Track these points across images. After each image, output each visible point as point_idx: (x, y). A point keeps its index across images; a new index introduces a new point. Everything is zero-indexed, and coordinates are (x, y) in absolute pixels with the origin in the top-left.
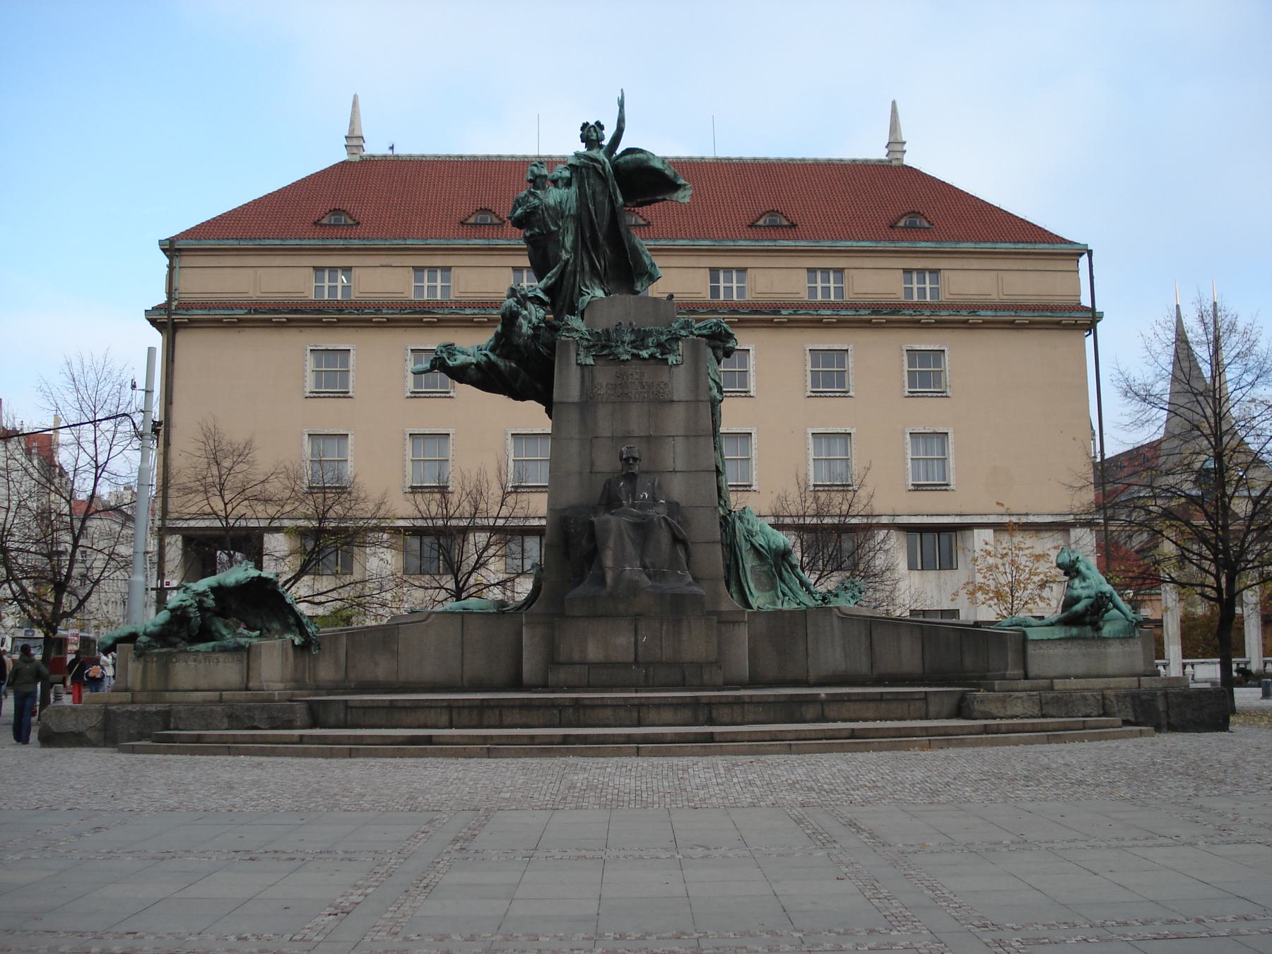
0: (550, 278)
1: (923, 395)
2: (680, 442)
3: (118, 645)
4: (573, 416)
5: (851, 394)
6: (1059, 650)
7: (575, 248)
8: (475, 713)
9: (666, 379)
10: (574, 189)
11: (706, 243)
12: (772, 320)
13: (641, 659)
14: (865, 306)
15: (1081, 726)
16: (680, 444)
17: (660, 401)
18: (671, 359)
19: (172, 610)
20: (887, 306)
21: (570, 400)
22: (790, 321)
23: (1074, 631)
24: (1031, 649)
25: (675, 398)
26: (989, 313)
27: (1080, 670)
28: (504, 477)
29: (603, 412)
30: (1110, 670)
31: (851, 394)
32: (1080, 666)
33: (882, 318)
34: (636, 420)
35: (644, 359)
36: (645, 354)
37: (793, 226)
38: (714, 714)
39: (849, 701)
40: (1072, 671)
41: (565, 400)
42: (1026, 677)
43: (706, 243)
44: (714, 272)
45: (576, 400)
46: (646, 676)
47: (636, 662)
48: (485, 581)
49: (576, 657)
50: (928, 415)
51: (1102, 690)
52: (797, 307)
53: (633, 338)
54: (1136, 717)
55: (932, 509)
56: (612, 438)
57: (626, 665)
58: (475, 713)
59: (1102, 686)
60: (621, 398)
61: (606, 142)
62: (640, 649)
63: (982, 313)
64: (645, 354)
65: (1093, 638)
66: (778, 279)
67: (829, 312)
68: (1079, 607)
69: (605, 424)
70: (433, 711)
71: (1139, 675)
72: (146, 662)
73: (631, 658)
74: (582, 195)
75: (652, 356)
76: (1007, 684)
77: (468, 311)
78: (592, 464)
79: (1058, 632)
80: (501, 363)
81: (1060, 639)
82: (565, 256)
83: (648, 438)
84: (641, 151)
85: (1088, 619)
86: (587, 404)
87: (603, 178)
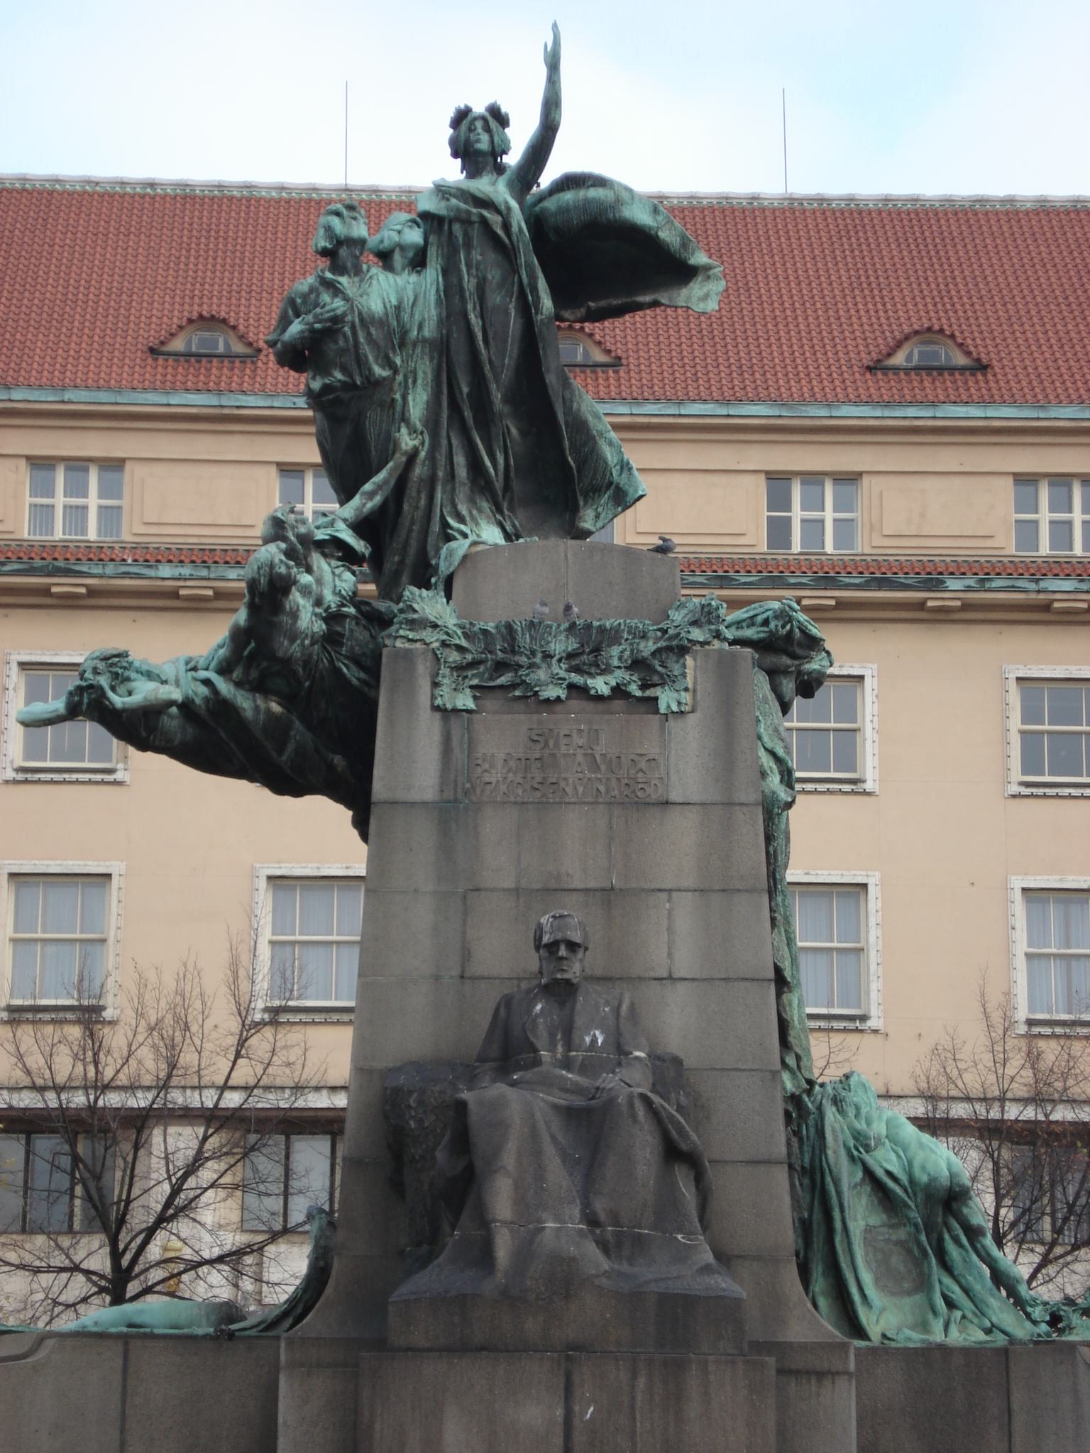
2: (685, 906)
4: (420, 837)
7: (432, 423)
9: (651, 748)
11: (759, 411)
12: (921, 605)
17: (638, 800)
18: (667, 699)
21: (415, 796)
22: (967, 606)
25: (675, 796)
28: (244, 986)
34: (578, 849)
35: (600, 698)
36: (601, 685)
37: (981, 367)
41: (401, 795)
43: (759, 411)
44: (778, 481)
48: (187, 1253)
52: (985, 572)
53: (572, 645)
60: (541, 794)
64: (601, 685)
67: (1068, 585)
69: (499, 852)
74: (451, 291)
75: (619, 692)
77: (166, 571)
78: (466, 955)
82: (407, 441)
84: (600, 182)
86: (455, 807)
87: (504, 249)
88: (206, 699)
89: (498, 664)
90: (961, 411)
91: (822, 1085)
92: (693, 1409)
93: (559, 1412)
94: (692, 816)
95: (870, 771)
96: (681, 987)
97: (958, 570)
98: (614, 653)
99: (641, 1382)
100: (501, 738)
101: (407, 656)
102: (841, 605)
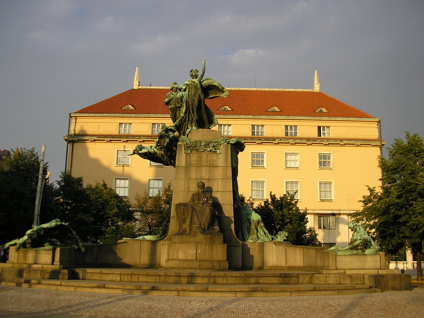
0: (177, 123)
1: (324, 169)
2: (220, 181)
3: (11, 247)
4: (183, 171)
5: (299, 168)
6: (349, 259)
7: (186, 113)
8: (129, 276)
9: (216, 159)
10: (187, 92)
13: (198, 259)
14: (304, 139)
15: (352, 288)
16: (220, 182)
17: (213, 166)
19: (28, 235)
20: (312, 139)
21: (182, 165)
23: (355, 252)
24: (338, 258)
25: (219, 165)
26: (347, 141)
27: (356, 267)
29: (193, 170)
30: (367, 267)
31: (299, 168)
32: (356, 266)
33: (310, 143)
34: (204, 174)
38: (216, 280)
39: (268, 276)
40: (353, 267)
41: (180, 165)
42: (336, 269)
45: (184, 165)
46: (200, 265)
47: (196, 260)
49: (175, 257)
50: (325, 175)
51: (363, 275)
53: (205, 144)
54: (376, 285)
55: (326, 208)
56: (196, 179)
57: (193, 261)
58: (129, 276)
59: (364, 273)
60: (199, 166)
61: (199, 77)
62: (198, 255)
63: (344, 141)
65: (362, 255)
66: (274, 127)
67: (292, 140)
68: (356, 243)
69: (193, 174)
70: (115, 275)
71: (378, 269)
72: (19, 253)
73: (195, 258)
75: (211, 150)
76: (328, 272)
78: (189, 188)
79: (348, 253)
80: (158, 152)
81: (349, 255)
83: (209, 179)
85: (359, 248)
86: (188, 167)
88: (153, 152)
89: (193, 147)
90: (278, 117)
91: (398, 192)
92: (215, 251)
93: (195, 251)
94: (221, 168)
95: (265, 165)
96: (219, 193)
97: (278, 138)
98: (211, 145)
99: (207, 247)
100: (194, 157)
101: (181, 145)
102: (262, 143)
